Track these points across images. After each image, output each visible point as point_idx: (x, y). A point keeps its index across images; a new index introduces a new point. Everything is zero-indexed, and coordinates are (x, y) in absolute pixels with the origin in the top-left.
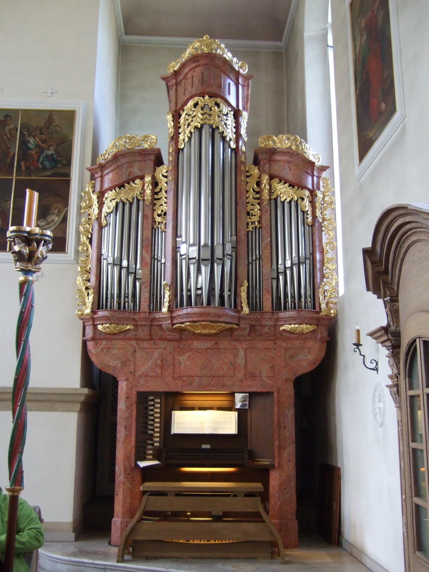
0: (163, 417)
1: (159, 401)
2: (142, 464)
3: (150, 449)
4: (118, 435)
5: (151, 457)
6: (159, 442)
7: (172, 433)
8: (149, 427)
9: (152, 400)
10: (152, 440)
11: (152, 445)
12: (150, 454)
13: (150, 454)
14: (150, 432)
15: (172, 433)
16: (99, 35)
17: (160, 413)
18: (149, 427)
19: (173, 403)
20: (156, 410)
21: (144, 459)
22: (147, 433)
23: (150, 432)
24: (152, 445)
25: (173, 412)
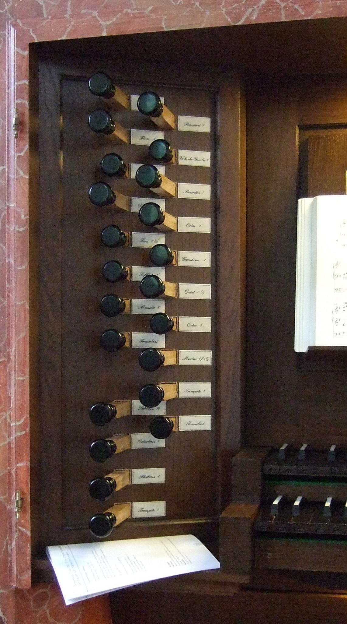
0: (234, 304)
1: (202, 124)
2: (87, 571)
3: (147, 458)
4: (25, 201)
5: (158, 508)
6: (213, 406)
7: (301, 346)
8: (138, 305)
9: (148, 120)
10: (152, 397)
11: (161, 428)
12: (149, 492)
13: (149, 492)
14: (139, 339)
15: (301, 346)
16: (329, 570)
17: (214, 309)
18: (138, 305)
19: (304, 146)
20: (191, 159)
21: (100, 530)
22: (114, 346)
23: (139, 339)
24: (161, 428)
25: (304, 204)
